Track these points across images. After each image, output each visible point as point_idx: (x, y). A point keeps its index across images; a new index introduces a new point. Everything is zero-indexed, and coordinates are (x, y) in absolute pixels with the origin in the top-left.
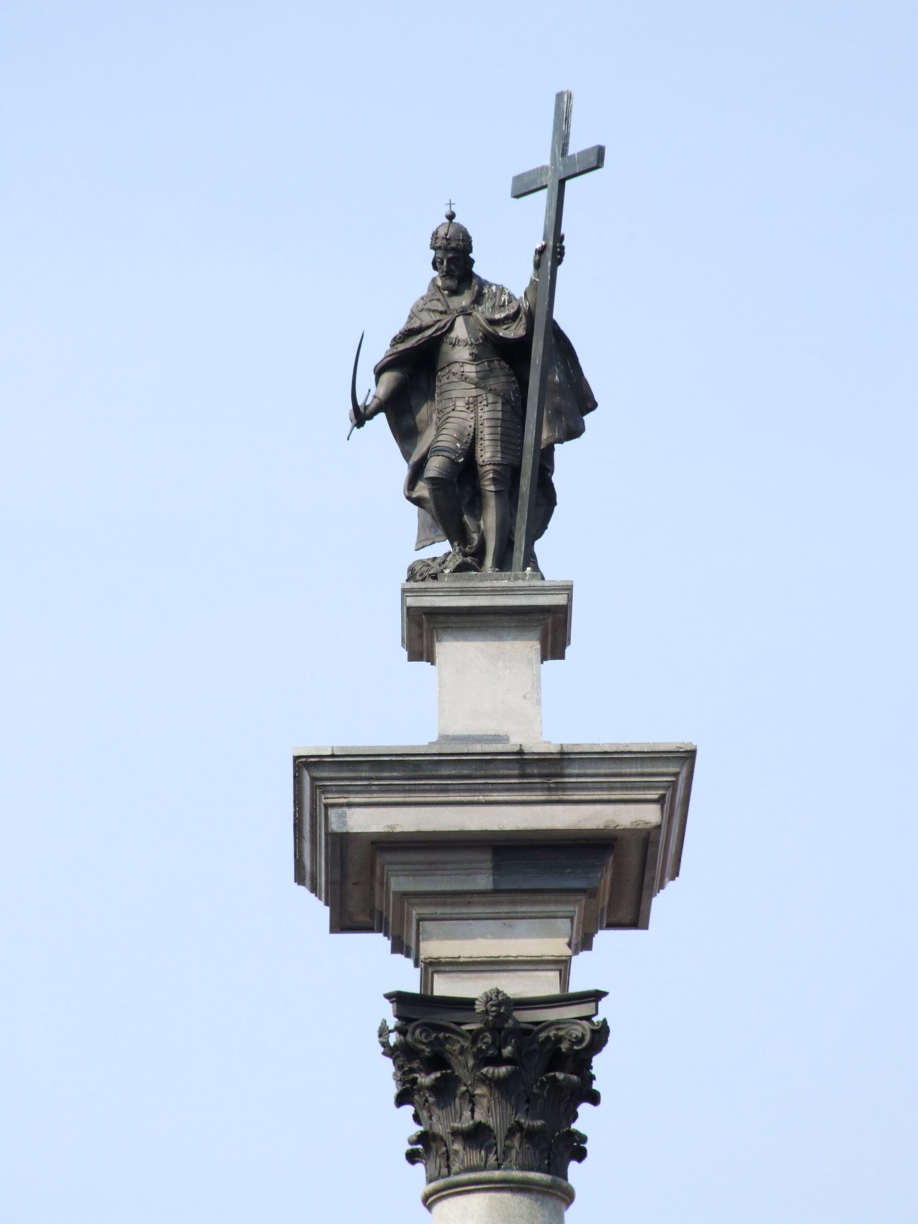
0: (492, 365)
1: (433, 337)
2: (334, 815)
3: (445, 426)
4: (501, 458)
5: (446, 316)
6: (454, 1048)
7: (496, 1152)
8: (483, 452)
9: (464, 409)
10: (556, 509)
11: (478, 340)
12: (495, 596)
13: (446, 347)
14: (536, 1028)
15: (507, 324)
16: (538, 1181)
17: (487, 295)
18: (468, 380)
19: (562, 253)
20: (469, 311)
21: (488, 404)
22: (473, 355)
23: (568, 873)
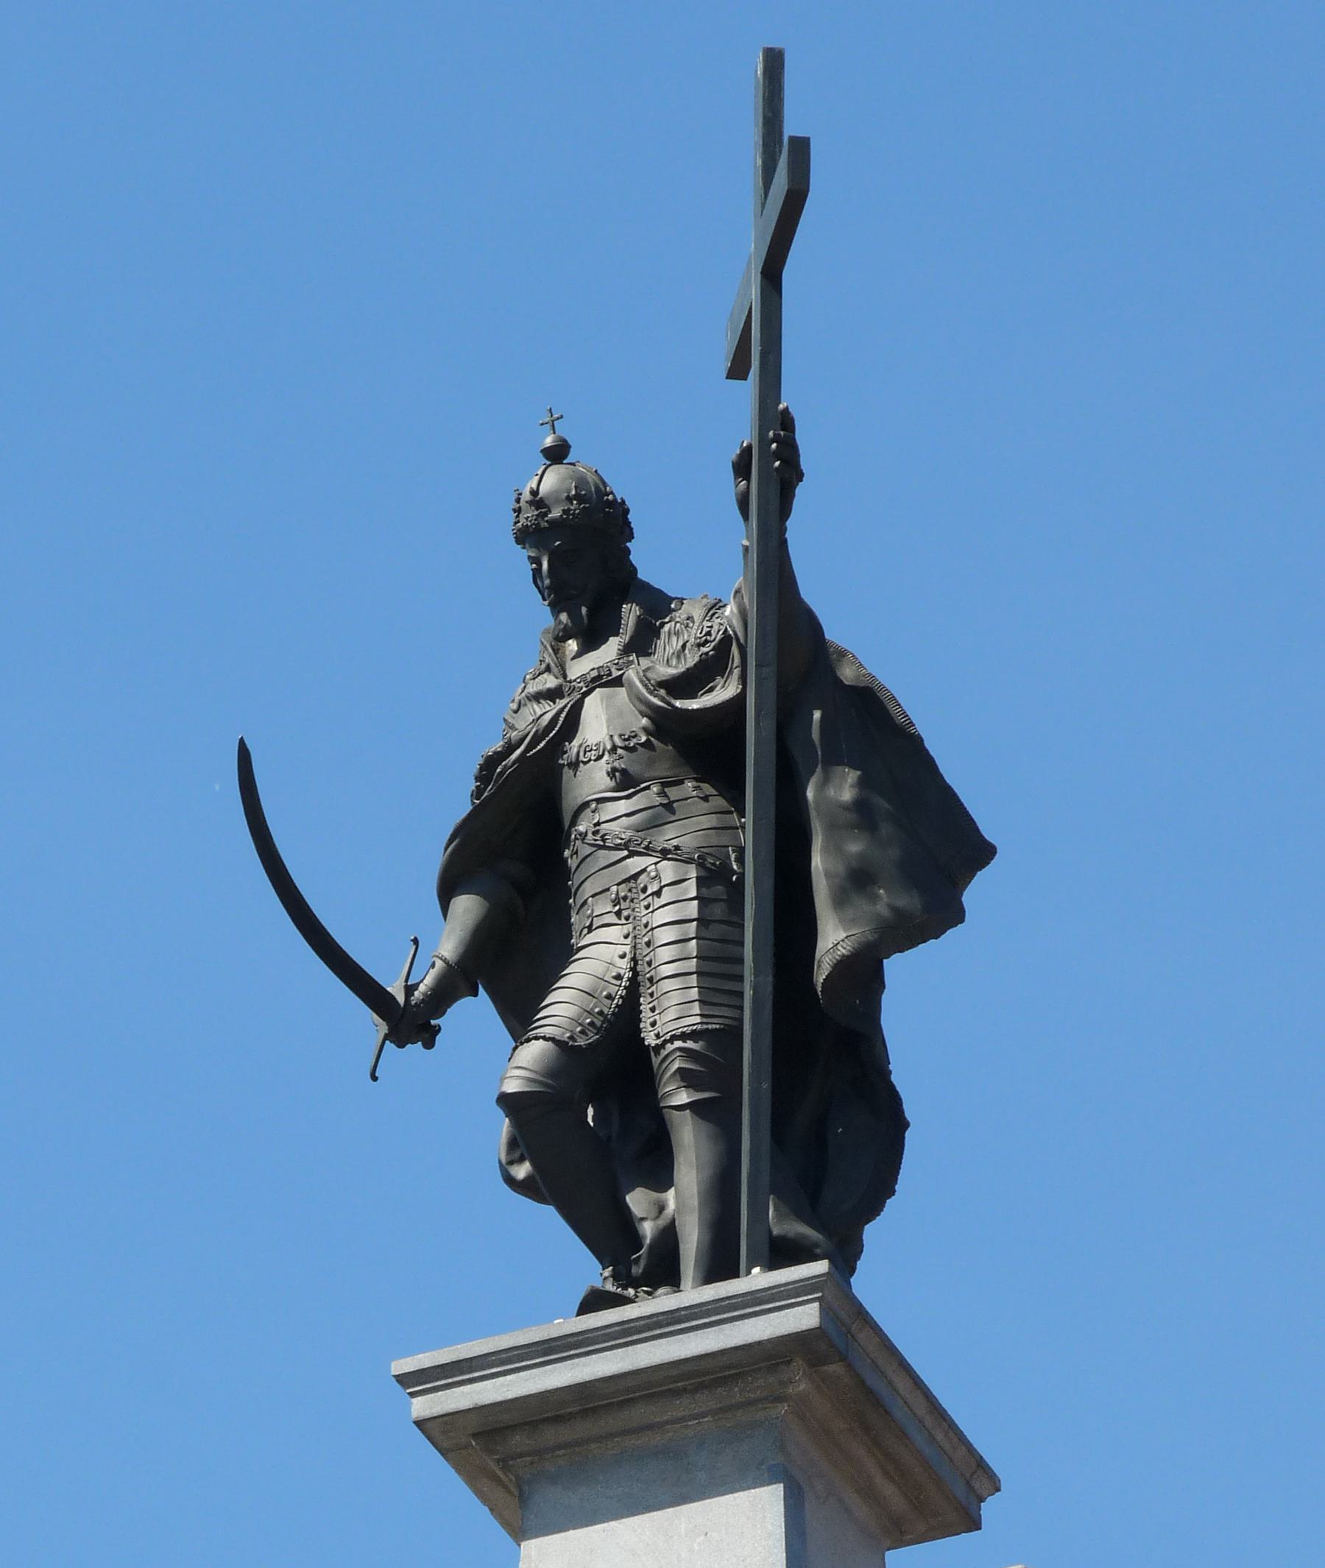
1: (621, 781)
4: (701, 1015)
9: (613, 919)
10: (909, 1134)
20: (616, 673)
21: (662, 888)
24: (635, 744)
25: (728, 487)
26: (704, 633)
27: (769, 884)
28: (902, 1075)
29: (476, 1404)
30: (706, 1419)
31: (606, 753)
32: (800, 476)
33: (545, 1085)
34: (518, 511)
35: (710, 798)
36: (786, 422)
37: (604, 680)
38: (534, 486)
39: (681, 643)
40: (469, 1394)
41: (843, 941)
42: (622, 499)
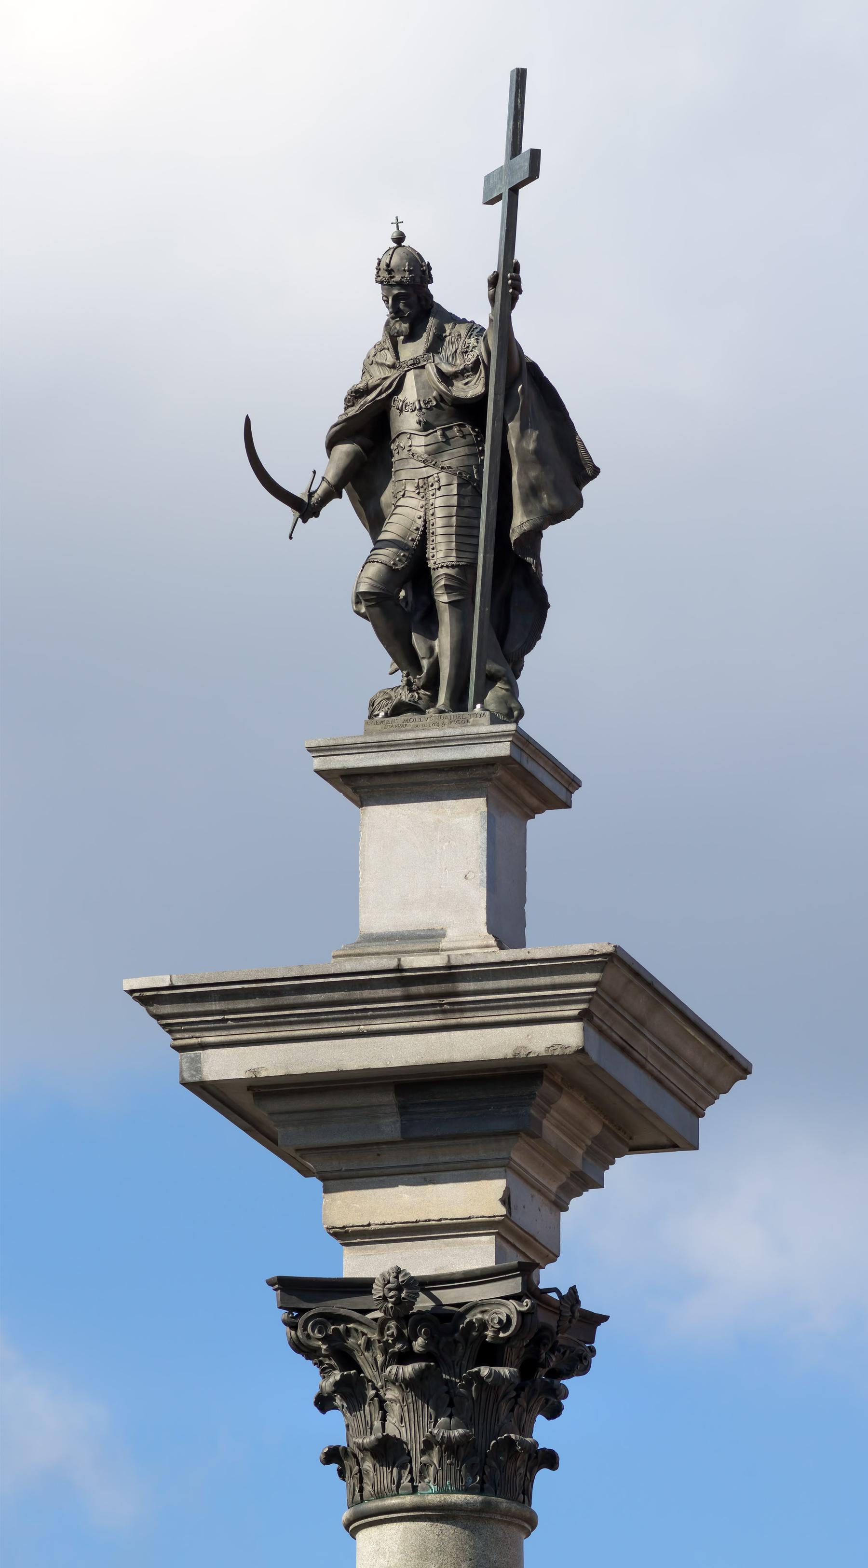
0: (448, 433)
2: (185, 1060)
4: (456, 557)
5: (395, 371)
6: (359, 1342)
7: (411, 1472)
8: (435, 551)
9: (414, 495)
10: (550, 611)
11: (431, 401)
12: (421, 750)
13: (394, 412)
14: (461, 1310)
15: (467, 377)
16: (462, 1505)
17: (447, 339)
18: (415, 458)
20: (422, 363)
22: (422, 424)
24: (431, 406)
25: (484, 290)
26: (466, 347)
27: (494, 507)
28: (547, 582)
29: (344, 767)
30: (452, 784)
31: (416, 410)
32: (520, 292)
33: (381, 589)
34: (378, 270)
35: (467, 436)
36: (516, 268)
37: (417, 365)
38: (388, 261)
39: (454, 350)
40: (341, 761)
41: (525, 522)
42: (428, 262)
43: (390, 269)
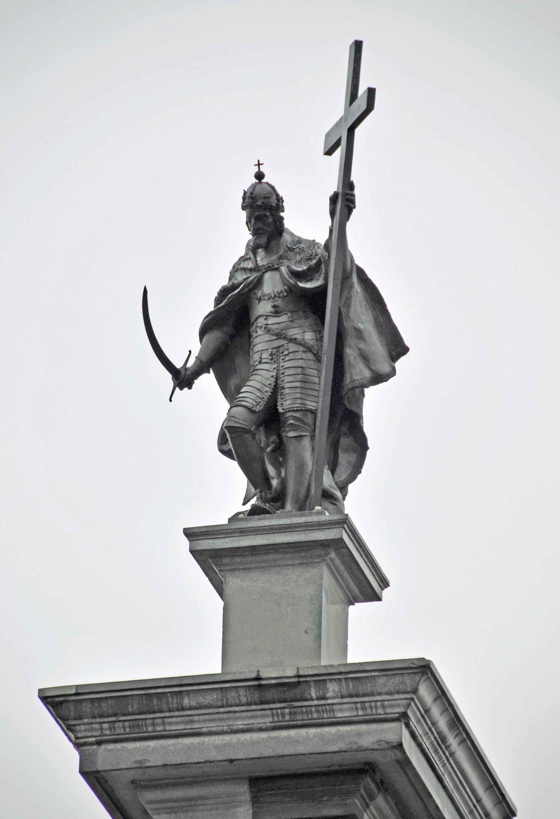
3: (252, 378)
10: (369, 452)
18: (271, 332)
19: (353, 202)
20: (276, 266)
23: (326, 800)
33: (454, 731)
36: (351, 186)
43: (253, 196)
